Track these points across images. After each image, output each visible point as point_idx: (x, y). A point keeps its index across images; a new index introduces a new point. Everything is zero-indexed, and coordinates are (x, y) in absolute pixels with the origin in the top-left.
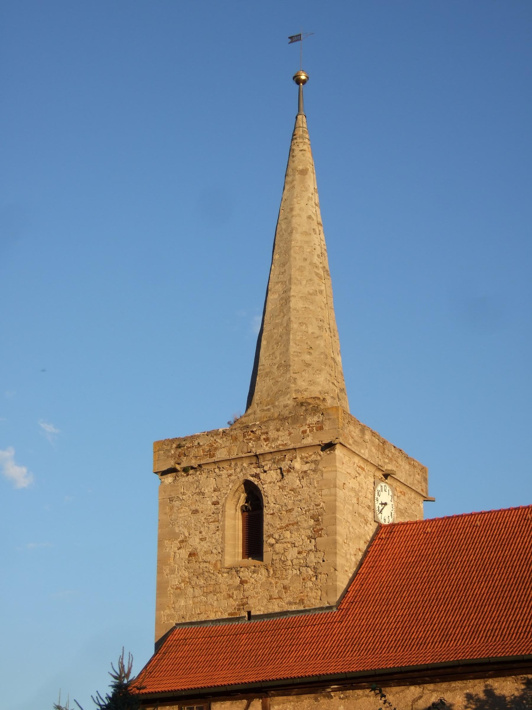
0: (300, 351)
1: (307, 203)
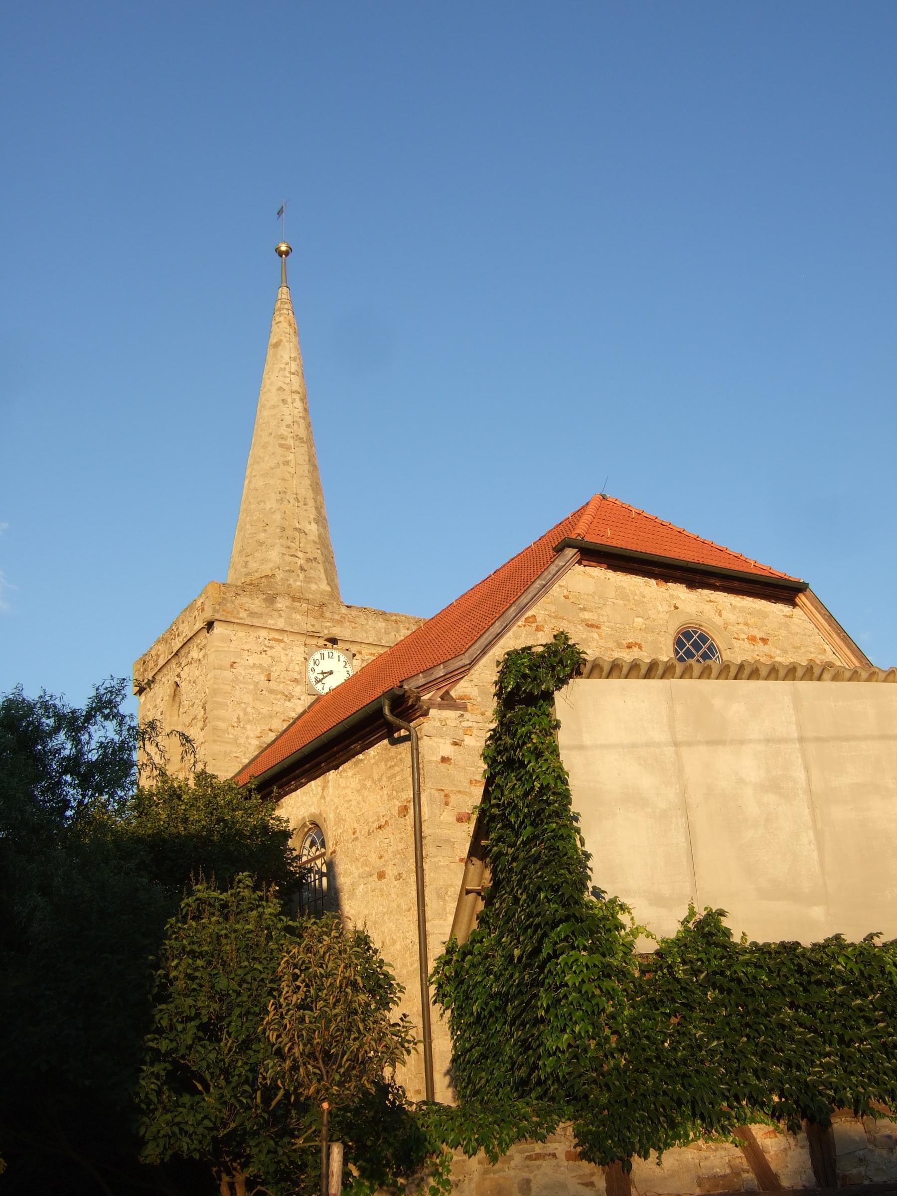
1: (282, 370)
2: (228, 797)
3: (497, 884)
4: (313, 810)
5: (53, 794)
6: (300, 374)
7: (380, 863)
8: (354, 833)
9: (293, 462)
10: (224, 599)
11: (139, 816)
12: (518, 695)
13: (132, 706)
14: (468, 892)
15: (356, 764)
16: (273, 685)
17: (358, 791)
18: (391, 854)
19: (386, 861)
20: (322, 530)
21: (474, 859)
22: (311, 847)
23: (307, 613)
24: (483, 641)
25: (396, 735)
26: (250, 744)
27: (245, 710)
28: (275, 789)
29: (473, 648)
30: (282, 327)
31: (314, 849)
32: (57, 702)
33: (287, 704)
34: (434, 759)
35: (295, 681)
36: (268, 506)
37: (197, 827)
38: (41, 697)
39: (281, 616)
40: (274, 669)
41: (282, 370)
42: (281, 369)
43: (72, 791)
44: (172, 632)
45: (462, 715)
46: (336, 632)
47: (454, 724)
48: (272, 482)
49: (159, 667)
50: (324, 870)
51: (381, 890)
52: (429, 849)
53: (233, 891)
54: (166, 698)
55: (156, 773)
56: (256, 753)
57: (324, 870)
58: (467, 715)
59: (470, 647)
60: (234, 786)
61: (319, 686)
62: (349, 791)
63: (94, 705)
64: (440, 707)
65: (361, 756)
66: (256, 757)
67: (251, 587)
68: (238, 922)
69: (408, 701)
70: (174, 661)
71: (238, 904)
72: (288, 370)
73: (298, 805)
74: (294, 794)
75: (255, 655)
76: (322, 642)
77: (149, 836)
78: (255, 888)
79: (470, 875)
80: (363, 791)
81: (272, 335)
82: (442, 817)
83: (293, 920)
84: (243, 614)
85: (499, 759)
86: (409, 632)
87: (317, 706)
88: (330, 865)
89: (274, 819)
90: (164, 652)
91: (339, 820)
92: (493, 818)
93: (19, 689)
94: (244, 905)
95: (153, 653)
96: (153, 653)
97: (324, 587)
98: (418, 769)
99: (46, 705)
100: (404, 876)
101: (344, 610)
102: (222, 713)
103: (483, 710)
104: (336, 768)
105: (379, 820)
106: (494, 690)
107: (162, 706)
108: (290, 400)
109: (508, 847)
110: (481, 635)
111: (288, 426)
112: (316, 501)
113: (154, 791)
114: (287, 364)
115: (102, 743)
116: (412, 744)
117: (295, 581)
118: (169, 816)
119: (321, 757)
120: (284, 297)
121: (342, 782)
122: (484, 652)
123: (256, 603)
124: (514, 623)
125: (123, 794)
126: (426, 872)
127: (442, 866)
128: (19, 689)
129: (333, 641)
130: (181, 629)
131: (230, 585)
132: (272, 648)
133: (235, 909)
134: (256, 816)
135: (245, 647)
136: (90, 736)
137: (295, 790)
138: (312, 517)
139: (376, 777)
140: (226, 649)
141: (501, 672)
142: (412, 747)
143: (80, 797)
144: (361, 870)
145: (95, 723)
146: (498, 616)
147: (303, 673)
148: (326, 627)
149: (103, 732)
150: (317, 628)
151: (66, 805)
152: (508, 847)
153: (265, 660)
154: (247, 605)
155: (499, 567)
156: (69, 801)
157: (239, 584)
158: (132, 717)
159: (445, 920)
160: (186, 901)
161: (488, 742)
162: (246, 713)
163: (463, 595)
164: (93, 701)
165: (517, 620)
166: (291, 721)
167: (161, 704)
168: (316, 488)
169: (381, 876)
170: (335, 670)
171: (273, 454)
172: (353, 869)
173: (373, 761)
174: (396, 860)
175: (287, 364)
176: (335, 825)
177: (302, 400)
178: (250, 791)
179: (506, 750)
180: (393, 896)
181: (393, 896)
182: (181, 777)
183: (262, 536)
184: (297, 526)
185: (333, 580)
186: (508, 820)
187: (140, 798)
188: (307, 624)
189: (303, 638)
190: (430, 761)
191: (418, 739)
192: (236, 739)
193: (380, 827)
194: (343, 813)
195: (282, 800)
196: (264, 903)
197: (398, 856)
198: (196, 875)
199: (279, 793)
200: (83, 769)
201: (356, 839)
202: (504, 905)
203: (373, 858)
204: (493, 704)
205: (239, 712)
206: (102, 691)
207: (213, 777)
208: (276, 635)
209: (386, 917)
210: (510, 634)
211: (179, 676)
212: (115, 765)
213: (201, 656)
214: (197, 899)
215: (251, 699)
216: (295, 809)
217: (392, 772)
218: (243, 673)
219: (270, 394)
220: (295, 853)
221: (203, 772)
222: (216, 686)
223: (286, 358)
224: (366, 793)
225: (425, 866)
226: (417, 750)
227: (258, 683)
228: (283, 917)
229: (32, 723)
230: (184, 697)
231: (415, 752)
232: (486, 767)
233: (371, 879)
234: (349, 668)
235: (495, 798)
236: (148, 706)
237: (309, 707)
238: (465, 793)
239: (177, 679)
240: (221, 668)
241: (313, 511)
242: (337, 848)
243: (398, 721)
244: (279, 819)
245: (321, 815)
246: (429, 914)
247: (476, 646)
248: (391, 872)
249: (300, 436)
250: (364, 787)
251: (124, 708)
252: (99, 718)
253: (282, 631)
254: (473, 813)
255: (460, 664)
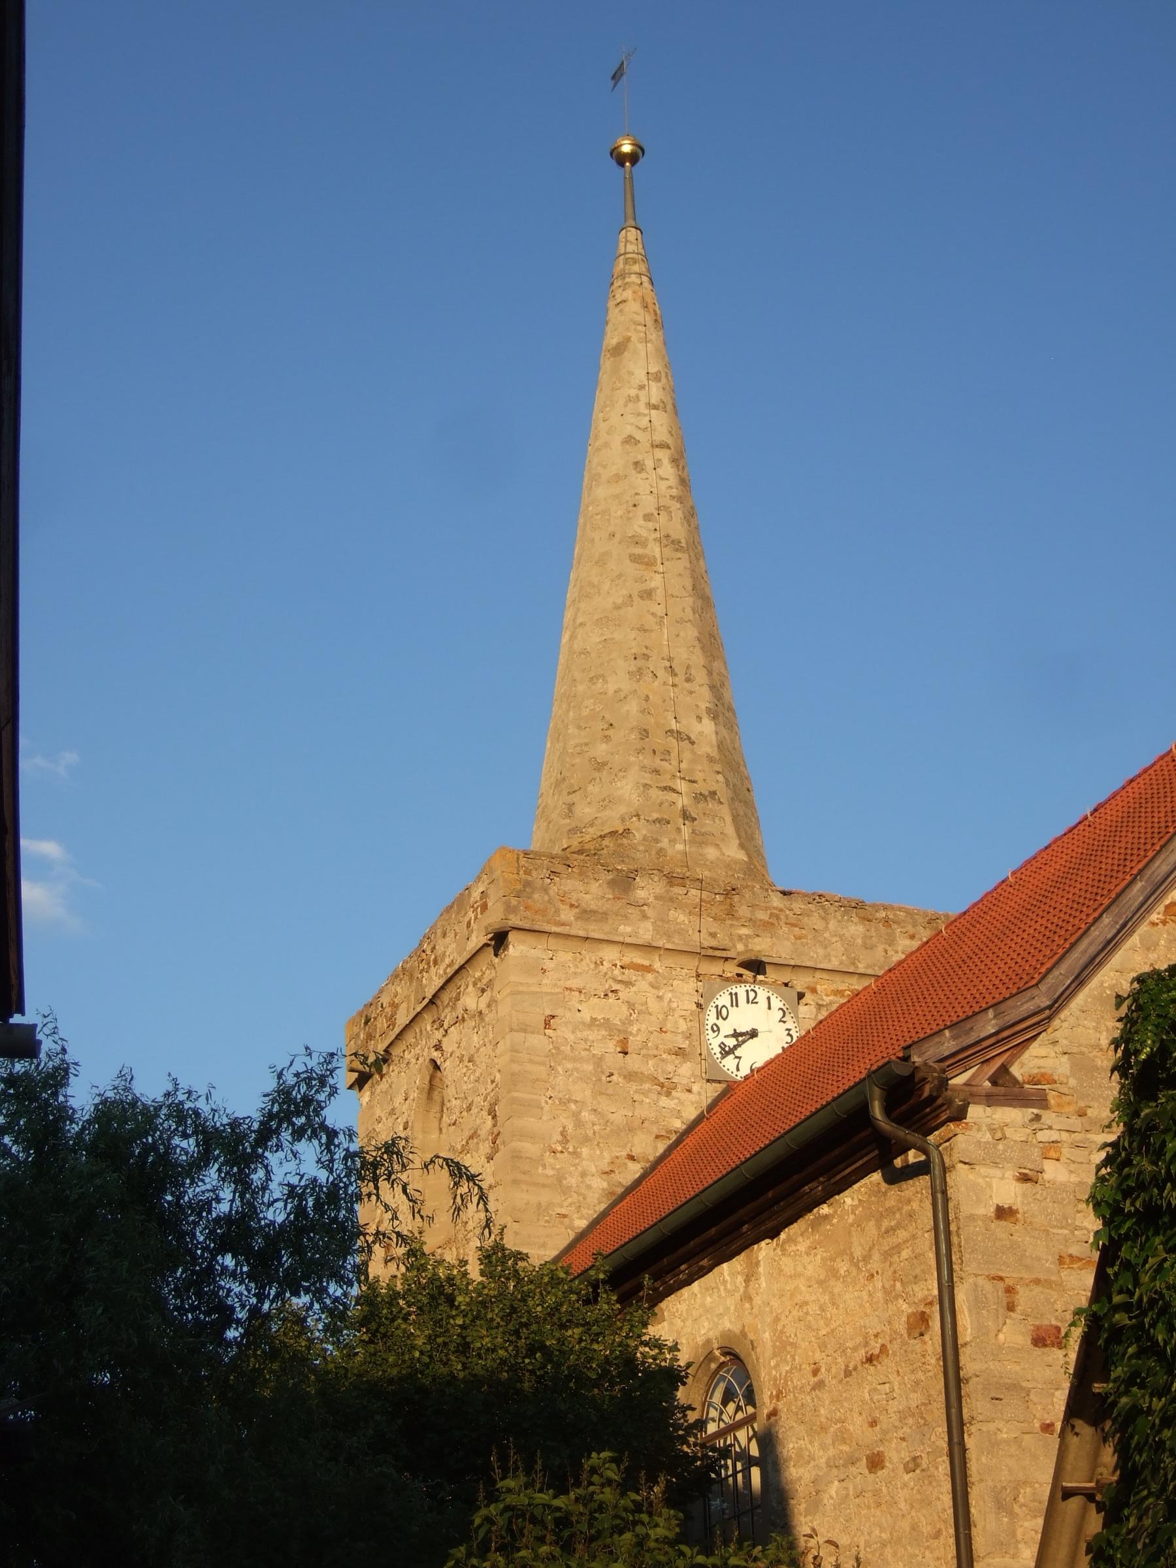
0: (586, 741)
1: (632, 401)
2: (550, 1300)
3: (1129, 1475)
4: (727, 1324)
5: (199, 1295)
6: (669, 407)
7: (871, 1435)
8: (815, 1372)
9: (660, 593)
10: (527, 884)
11: (371, 1342)
12: (1164, 1069)
13: (343, 1110)
14: (1068, 1494)
15: (815, 1225)
16: (633, 1062)
17: (820, 1283)
18: (895, 1418)
19: (885, 1432)
20: (724, 732)
21: (1080, 1424)
22: (725, 1403)
23: (699, 909)
24: (1077, 958)
25: (898, 1162)
26: (589, 1187)
27: (576, 1115)
28: (647, 1280)
29: (1056, 973)
30: (629, 312)
31: (731, 1407)
32: (201, 1105)
33: (664, 1101)
34: (981, 1211)
35: (680, 1052)
36: (611, 688)
37: (489, 1362)
38: (167, 1095)
39: (645, 917)
40: (634, 1029)
41: (632, 401)
42: (629, 399)
43: (237, 1288)
44: (423, 956)
45: (1038, 1118)
46: (762, 946)
47: (1020, 1135)
48: (618, 636)
49: (397, 1030)
50: (754, 1451)
51: (876, 1493)
52: (975, 1405)
53: (580, 1491)
54: (414, 1094)
55: (401, 1251)
56: (603, 1207)
57: (754, 1451)
58: (1048, 1117)
59: (1049, 971)
60: (562, 1275)
61: (729, 1063)
62: (801, 1284)
63: (276, 1108)
64: (990, 1100)
65: (824, 1209)
66: (604, 1215)
67: (581, 857)
68: (595, 1557)
69: (921, 1089)
70: (428, 1017)
71: (592, 1519)
72: (643, 400)
73: (695, 1314)
74: (685, 1292)
75: (596, 1000)
76: (732, 969)
77: (391, 1381)
78: (627, 1484)
79: (1071, 1457)
80: (832, 1282)
81: (609, 328)
82: (1001, 1336)
83: (708, 1552)
84: (567, 915)
85: (1128, 1207)
86: (916, 944)
87: (726, 1106)
88: (768, 1441)
89: (646, 1344)
90: (407, 997)
91: (783, 1345)
92: (1117, 1334)
93: (126, 1078)
94: (605, 1521)
95: (385, 1000)
96: (385, 1000)
97: (734, 852)
98: (948, 1233)
99: (182, 1111)
100: (924, 1463)
101: (776, 901)
102: (529, 1122)
103: (1082, 1104)
104: (774, 1234)
105: (866, 1344)
106: (1109, 1058)
107: (406, 1111)
108: (649, 464)
109: (1152, 1396)
110: (1073, 945)
111: (648, 517)
112: (710, 673)
113: (399, 1287)
114: (641, 387)
115: (292, 1187)
116: (933, 1181)
117: (672, 841)
118: (430, 1339)
119: (742, 1212)
120: (630, 248)
121: (787, 1264)
122: (1080, 980)
123: (594, 892)
124: (1142, 918)
125: (339, 1293)
126: (972, 1454)
127: (1007, 1442)
128: (126, 1078)
129: (756, 966)
130: (440, 949)
131: (538, 855)
132: (628, 984)
133: (585, 1528)
134: (609, 1339)
135: (574, 983)
136: (268, 1173)
137: (689, 1282)
138: (703, 706)
139: (858, 1252)
140: (535, 989)
141: (1128, 1020)
142: (933, 1187)
143: (254, 1300)
144: (832, 1452)
145: (279, 1147)
146: (1106, 902)
147: (696, 1034)
148: (740, 937)
149: (294, 1165)
150: (722, 939)
151: (227, 1317)
152: (1152, 1396)
153: (615, 1010)
154: (574, 896)
155: (1102, 799)
156: (232, 1308)
157: (557, 850)
158: (351, 1134)
159: (1014, 1557)
160: (483, 1512)
161: (1103, 1171)
162: (579, 1124)
163: (1028, 862)
164: (274, 1101)
165: (1149, 911)
166: (674, 1137)
167: (404, 1108)
168: (710, 644)
169: (876, 1463)
170: (760, 1029)
171: (620, 576)
172: (815, 1448)
173: (851, 1218)
174: (907, 1430)
175: (641, 387)
176: (774, 1355)
177: (674, 461)
178: (595, 1285)
179: (1142, 1186)
180: (902, 1505)
181: (902, 1505)
182: (450, 1257)
183: (600, 750)
184: (674, 725)
185: (751, 838)
186: (1151, 1339)
187: (369, 1300)
188: (699, 930)
189: (692, 963)
190: (972, 1218)
191: (945, 1170)
192: (560, 1178)
193: (870, 1360)
194: (790, 1331)
195: (663, 1305)
196: (645, 1517)
197: (910, 1421)
198: (503, 1458)
199: (655, 1290)
200: (258, 1243)
201: (820, 1385)
202: (1147, 1522)
203: (857, 1425)
204: (1111, 1088)
205: (565, 1122)
206: (290, 1080)
207: (520, 1256)
208: (638, 958)
209: (888, 1551)
210: (1135, 939)
211: (438, 1047)
212: (322, 1234)
213: (482, 1006)
214: (508, 1508)
215: (588, 1093)
216: (689, 1323)
217: (892, 1240)
218: (571, 1037)
219: (607, 453)
220: (692, 1417)
221: (498, 1247)
222: (516, 1067)
223: (640, 375)
224: (838, 1287)
225: (970, 1442)
226: (944, 1192)
227: (601, 1059)
228: (685, 1548)
229: (154, 1147)
230: (450, 1092)
231: (941, 1198)
232: (1098, 1225)
233: (853, 1470)
234: (790, 1024)
235: (1120, 1292)
236: (378, 1112)
237: (711, 1107)
238: (1048, 1284)
239: (436, 1055)
240: (524, 1029)
241: (706, 692)
242: (780, 1405)
243: (902, 1133)
244: (657, 1344)
245: (744, 1334)
246: (980, 1542)
247: (1063, 968)
248: (896, 1455)
249: (674, 536)
250: (834, 1273)
251: (336, 1114)
252: (286, 1136)
253: (648, 948)
254: (1073, 1324)
255: (1030, 1006)
